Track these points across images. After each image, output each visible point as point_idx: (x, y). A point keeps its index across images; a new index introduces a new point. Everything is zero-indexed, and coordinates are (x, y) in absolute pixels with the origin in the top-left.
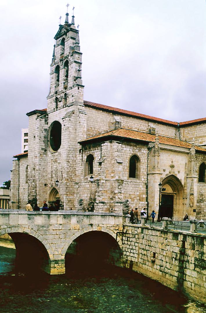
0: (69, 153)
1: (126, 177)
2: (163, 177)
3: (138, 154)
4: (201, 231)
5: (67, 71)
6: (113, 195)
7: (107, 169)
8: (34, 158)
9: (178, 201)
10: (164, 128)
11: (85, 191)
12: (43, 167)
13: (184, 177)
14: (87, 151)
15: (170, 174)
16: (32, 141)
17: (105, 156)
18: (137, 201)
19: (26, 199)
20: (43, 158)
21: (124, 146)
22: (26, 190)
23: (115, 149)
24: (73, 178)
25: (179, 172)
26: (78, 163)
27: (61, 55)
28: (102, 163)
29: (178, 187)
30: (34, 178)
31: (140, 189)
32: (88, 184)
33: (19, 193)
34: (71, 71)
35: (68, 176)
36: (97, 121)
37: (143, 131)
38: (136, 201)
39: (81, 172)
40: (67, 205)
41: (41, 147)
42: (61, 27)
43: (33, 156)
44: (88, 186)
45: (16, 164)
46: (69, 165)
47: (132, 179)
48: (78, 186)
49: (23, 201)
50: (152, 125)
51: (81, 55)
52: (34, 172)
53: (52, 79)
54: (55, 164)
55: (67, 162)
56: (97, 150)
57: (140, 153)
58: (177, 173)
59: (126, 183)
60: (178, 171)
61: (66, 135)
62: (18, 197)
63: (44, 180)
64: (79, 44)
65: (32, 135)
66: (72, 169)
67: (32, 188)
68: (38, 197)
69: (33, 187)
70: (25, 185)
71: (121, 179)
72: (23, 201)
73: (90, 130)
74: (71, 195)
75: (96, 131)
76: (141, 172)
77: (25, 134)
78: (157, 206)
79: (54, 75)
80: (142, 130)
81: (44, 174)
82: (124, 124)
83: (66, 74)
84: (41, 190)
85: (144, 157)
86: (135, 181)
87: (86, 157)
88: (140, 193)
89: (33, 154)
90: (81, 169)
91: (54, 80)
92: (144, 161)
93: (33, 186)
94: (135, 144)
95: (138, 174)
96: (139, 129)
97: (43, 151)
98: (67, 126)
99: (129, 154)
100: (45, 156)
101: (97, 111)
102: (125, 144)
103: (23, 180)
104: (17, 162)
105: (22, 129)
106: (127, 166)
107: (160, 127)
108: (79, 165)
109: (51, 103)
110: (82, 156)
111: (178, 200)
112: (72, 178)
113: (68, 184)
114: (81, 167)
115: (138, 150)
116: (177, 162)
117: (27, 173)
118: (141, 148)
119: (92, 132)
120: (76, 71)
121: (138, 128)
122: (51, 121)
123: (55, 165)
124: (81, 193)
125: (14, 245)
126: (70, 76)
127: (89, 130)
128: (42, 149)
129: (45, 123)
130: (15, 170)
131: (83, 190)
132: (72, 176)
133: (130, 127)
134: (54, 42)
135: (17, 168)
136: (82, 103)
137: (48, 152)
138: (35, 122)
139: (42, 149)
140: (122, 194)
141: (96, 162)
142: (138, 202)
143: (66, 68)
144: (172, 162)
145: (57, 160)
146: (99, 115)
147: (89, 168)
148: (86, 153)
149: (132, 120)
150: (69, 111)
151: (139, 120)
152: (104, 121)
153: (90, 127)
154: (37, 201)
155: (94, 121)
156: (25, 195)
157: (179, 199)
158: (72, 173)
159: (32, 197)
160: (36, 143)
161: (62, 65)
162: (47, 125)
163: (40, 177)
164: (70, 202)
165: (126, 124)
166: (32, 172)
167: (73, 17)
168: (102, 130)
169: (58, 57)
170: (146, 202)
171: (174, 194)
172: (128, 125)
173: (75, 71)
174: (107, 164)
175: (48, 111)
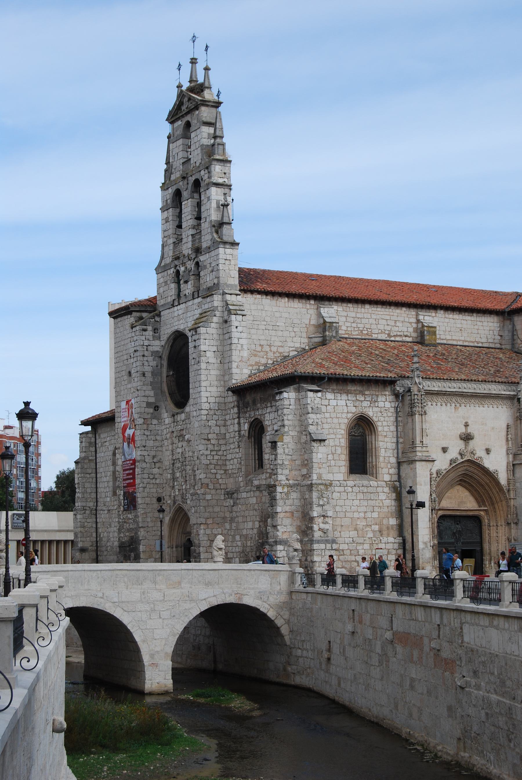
1: (342, 475)
2: (444, 468)
3: (371, 413)
5: (199, 205)
9: (493, 530)
10: (465, 322)
12: (153, 453)
13: (505, 464)
14: (249, 409)
15: (462, 458)
18: (374, 536)
20: (151, 427)
21: (330, 396)
22: (114, 515)
24: (220, 480)
25: (488, 451)
26: (231, 440)
27: (183, 163)
29: (490, 492)
31: (381, 505)
32: (254, 496)
35: (209, 475)
36: (274, 328)
37: (404, 338)
40: (207, 552)
41: (145, 399)
42: (181, 95)
44: (254, 500)
46: (210, 447)
47: (358, 480)
48: (232, 501)
49: (109, 544)
50: (426, 318)
51: (228, 165)
53: (166, 222)
54: (180, 445)
55: (205, 439)
56: (269, 410)
57: (375, 409)
58: (480, 453)
59: (342, 489)
62: (94, 535)
64: (222, 137)
65: (124, 368)
66: (216, 457)
68: (142, 533)
70: (111, 500)
71: (324, 482)
72: (109, 544)
73: (259, 352)
74: (216, 526)
75: (274, 353)
76: (381, 459)
78: (427, 547)
79: (171, 214)
80: (400, 336)
81: (156, 471)
82: (349, 324)
83: (198, 212)
84: (149, 515)
85: (386, 419)
86: (365, 483)
87: (247, 427)
88: (382, 515)
91: (171, 227)
92: (386, 429)
94: (358, 388)
95: (374, 463)
96: (392, 334)
97: (151, 410)
99: (344, 416)
100: (155, 422)
101: (275, 301)
102: (333, 391)
103: (105, 488)
104: (90, 438)
106: (342, 447)
107: (452, 321)
108: (232, 446)
109: (166, 282)
110: (239, 423)
111: (495, 528)
113: (209, 497)
114: (237, 450)
115: (369, 403)
116: (483, 424)
117: (115, 468)
118: (377, 396)
119: (263, 357)
121: (387, 332)
122: (167, 331)
123: (180, 446)
124: (240, 519)
125: (83, 657)
126: (206, 218)
127: (257, 351)
128: (149, 405)
129: (154, 336)
130: (86, 461)
131: (244, 511)
132: (218, 476)
133: (366, 332)
134: (167, 128)
136: (236, 286)
137: (164, 411)
138: (130, 335)
139: (149, 405)
140: (330, 520)
142: (377, 538)
143: (196, 196)
144: (466, 425)
145: (184, 432)
146: (281, 309)
147: (257, 453)
148: (248, 415)
149: (370, 311)
151: (391, 310)
152: (293, 325)
153: (258, 343)
154: (140, 544)
155: (267, 327)
156: (112, 529)
157: (497, 526)
158: (217, 467)
159: (127, 534)
160: (133, 390)
161: (187, 189)
162: (157, 343)
165: (354, 325)
167: (207, 69)
168: (291, 349)
169: (177, 164)
170: (400, 537)
171: (482, 513)
172: (359, 325)
175: (160, 302)
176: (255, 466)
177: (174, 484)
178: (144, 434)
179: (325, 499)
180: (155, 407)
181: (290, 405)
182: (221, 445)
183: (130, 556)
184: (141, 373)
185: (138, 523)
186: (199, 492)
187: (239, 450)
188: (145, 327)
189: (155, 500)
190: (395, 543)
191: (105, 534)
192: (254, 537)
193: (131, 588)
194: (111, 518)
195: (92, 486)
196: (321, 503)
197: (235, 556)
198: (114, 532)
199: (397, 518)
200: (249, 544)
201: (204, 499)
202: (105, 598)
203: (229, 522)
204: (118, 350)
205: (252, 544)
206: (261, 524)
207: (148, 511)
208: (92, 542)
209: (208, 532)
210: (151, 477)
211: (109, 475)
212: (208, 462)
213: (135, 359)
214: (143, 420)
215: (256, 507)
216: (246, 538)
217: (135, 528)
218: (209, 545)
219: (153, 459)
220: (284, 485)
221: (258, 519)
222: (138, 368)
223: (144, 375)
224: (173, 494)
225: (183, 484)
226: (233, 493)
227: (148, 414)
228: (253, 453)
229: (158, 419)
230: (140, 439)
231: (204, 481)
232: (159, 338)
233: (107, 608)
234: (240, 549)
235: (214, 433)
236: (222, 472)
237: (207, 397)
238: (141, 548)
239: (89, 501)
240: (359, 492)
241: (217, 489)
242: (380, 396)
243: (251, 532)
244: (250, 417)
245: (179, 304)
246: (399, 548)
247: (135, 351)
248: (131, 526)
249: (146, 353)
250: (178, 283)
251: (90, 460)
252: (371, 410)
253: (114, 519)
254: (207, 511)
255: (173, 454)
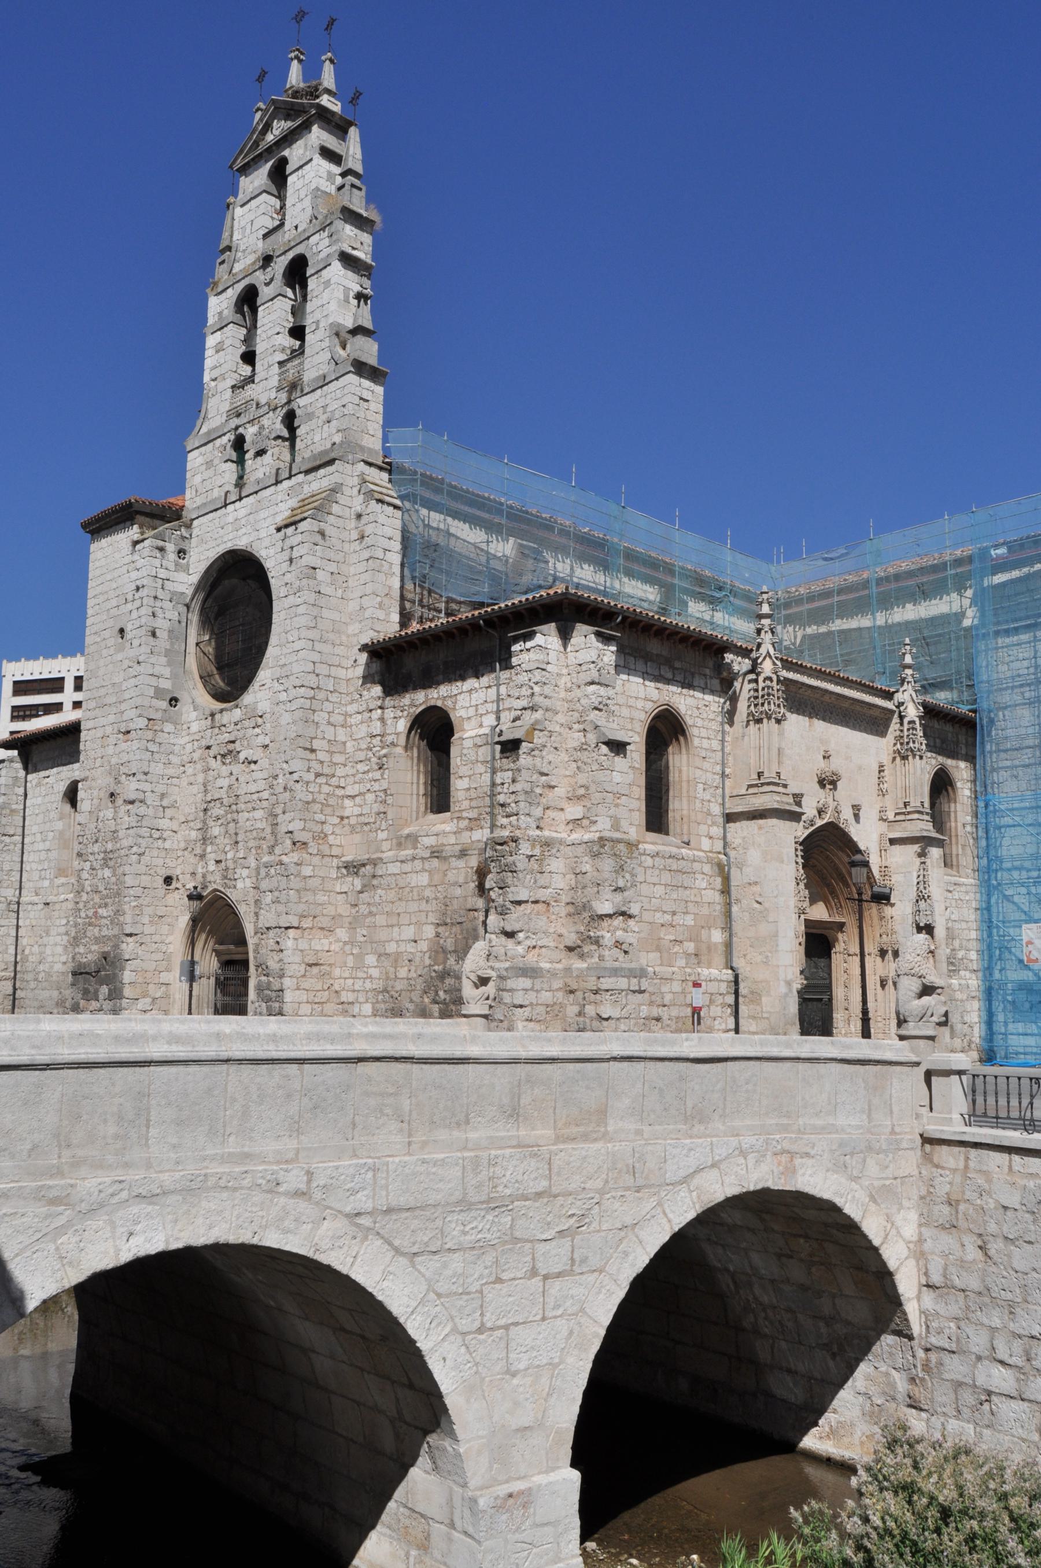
0: (316, 705)
4: (985, 1115)
6: (582, 929)
7: (544, 778)
8: (112, 740)
11: (400, 906)
12: (160, 789)
16: (105, 653)
17: (533, 708)
19: (56, 959)
20: (161, 737)
22: (56, 914)
23: (584, 668)
24: (331, 838)
26: (361, 755)
28: (524, 744)
30: (110, 846)
32: (424, 870)
33: (18, 927)
34: (320, 303)
35: (310, 825)
38: (682, 962)
39: (376, 807)
40: (298, 989)
41: (153, 681)
43: (109, 730)
45: (10, 781)
52: (109, 813)
55: (306, 749)
60: (853, 806)
61: (302, 609)
62: (12, 950)
63: (163, 854)
66: (326, 789)
67: (97, 899)
69: (105, 892)
71: (625, 836)
72: (41, 967)
77: (15, 683)
78: (790, 991)
89: (112, 718)
90: (376, 786)
93: (101, 888)
97: (164, 704)
98: (304, 561)
100: (168, 727)
103: (40, 861)
105: (5, 662)
112: (326, 835)
113: (307, 871)
114: (377, 775)
118: (693, 674)
120: (347, 301)
126: (317, 322)
128: (159, 693)
132: (328, 829)
135: (14, 797)
138: (130, 558)
139: (159, 693)
141: (468, 743)
145: (237, 746)
150: (307, 490)
154: (123, 969)
156: (51, 940)
158: (327, 811)
159: (94, 948)
160: (126, 663)
162: (181, 576)
163: (140, 840)
164: (315, 970)
166: (101, 814)
173: (342, 297)
174: (544, 753)
176: (418, 807)
177: (204, 850)
178: (147, 750)
179: (628, 876)
180: (171, 700)
181: (548, 663)
182: (335, 764)
183: (96, 992)
184: (150, 629)
185: (121, 925)
186: (284, 859)
187: (382, 775)
188: (161, 543)
189: (161, 881)
190: (721, 981)
191: (36, 949)
192: (418, 959)
193: (424, 1144)
194: (50, 918)
195: (14, 858)
196: (621, 883)
197: (361, 1000)
198: (56, 945)
199: (723, 928)
200: (403, 973)
201: (298, 875)
202: (318, 1195)
203: (347, 925)
204: (15, 714)
205: (413, 975)
206: (441, 929)
207: (145, 903)
208: (6, 963)
209: (303, 945)
210: (155, 836)
211: (50, 838)
212: (310, 798)
213: (138, 603)
214: (146, 722)
215: (427, 893)
216: (396, 961)
217: (115, 936)
218: (302, 972)
219: (161, 800)
220: (534, 840)
221: (432, 918)
222: (143, 620)
223: (154, 634)
224: (200, 870)
225: (227, 849)
226: (364, 865)
227: (157, 710)
228: (415, 781)
229: (175, 723)
230: (138, 757)
231: (299, 836)
232: (186, 569)
233: (325, 1245)
234: (379, 985)
235: (324, 738)
236: (337, 820)
237: (314, 663)
238: (127, 976)
239: (5, 885)
240: (665, 869)
241: (323, 856)
242: (697, 676)
243: (410, 948)
244: (412, 705)
245: (240, 499)
246: (728, 993)
247: (138, 589)
248: (105, 932)
249: (160, 594)
250: (240, 462)
251: (13, 811)
252: (682, 701)
253: (58, 921)
254: (304, 900)
255: (206, 791)
